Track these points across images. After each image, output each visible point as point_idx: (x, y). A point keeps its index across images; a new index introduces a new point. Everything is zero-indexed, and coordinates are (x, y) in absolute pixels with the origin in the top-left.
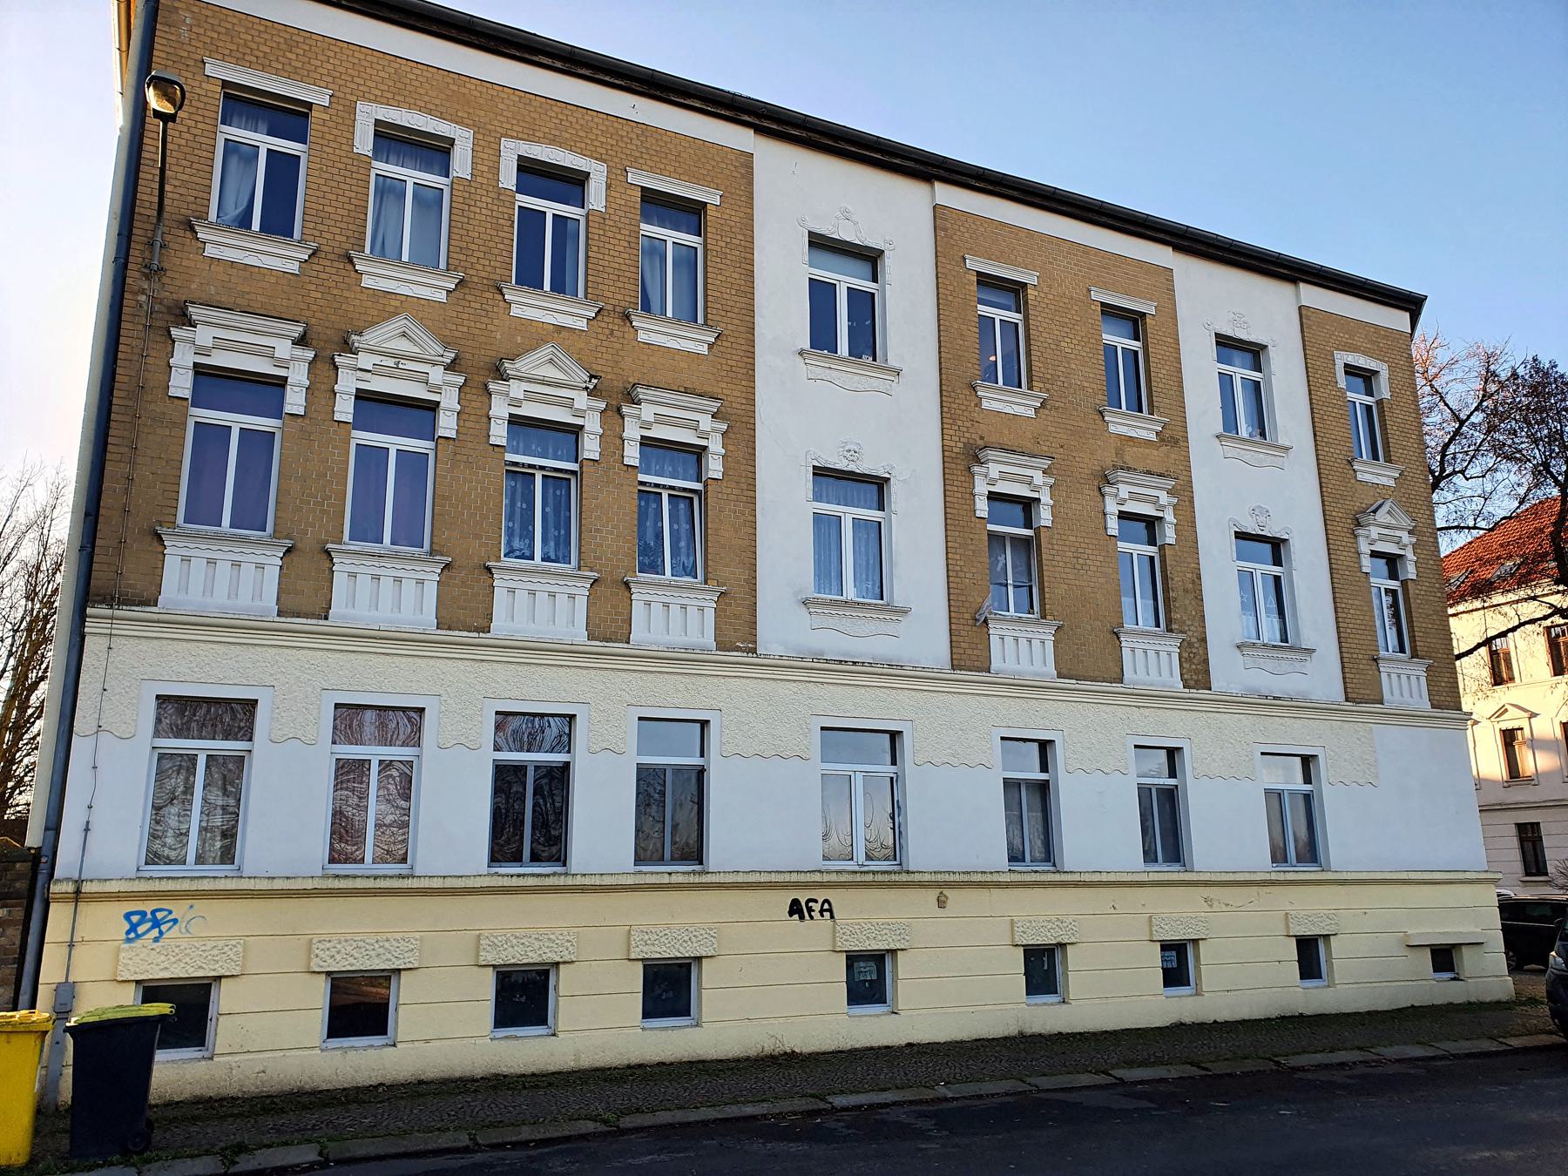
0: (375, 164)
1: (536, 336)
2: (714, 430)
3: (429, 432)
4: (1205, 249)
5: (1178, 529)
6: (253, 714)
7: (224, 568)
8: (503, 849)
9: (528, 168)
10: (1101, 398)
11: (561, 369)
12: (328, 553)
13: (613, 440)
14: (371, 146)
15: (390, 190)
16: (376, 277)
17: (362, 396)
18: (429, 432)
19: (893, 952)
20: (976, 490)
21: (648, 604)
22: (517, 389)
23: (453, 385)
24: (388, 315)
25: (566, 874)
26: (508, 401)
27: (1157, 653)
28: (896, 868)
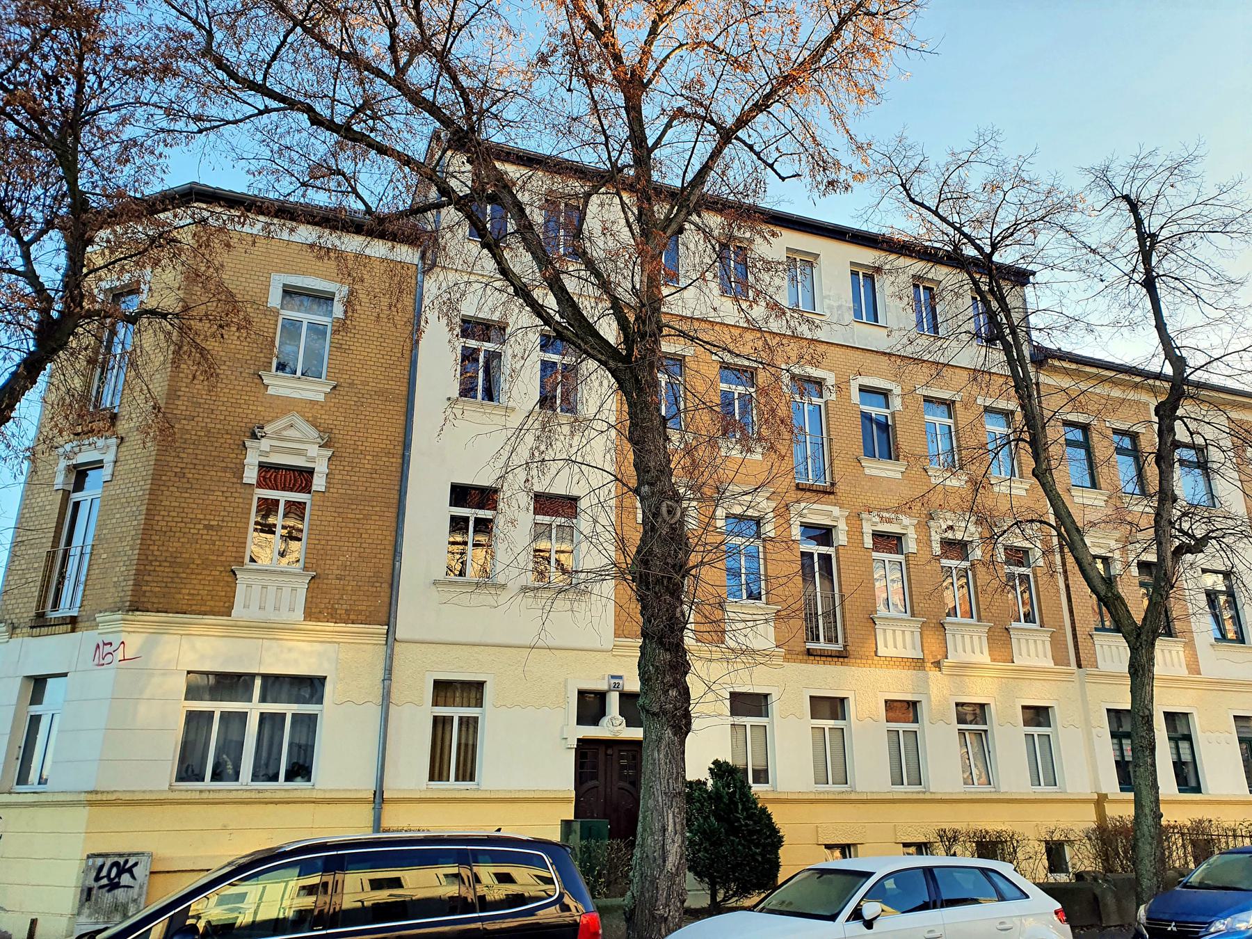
0: (282, 312)
1: (286, 406)
2: (842, 516)
3: (307, 488)
4: (1128, 378)
5: (918, 541)
6: (323, 685)
7: (272, 589)
8: (437, 772)
9: (289, 292)
10: (860, 452)
11: (298, 429)
12: (233, 572)
13: (925, 541)
14: (279, 302)
15: (292, 328)
16: (279, 386)
17: (263, 467)
18: (307, 488)
19: (855, 845)
20: (864, 530)
21: (1019, 640)
22: (265, 444)
23: (323, 456)
24: (284, 412)
25: (478, 790)
26: (258, 453)
27: (1035, 641)
28: (849, 789)
